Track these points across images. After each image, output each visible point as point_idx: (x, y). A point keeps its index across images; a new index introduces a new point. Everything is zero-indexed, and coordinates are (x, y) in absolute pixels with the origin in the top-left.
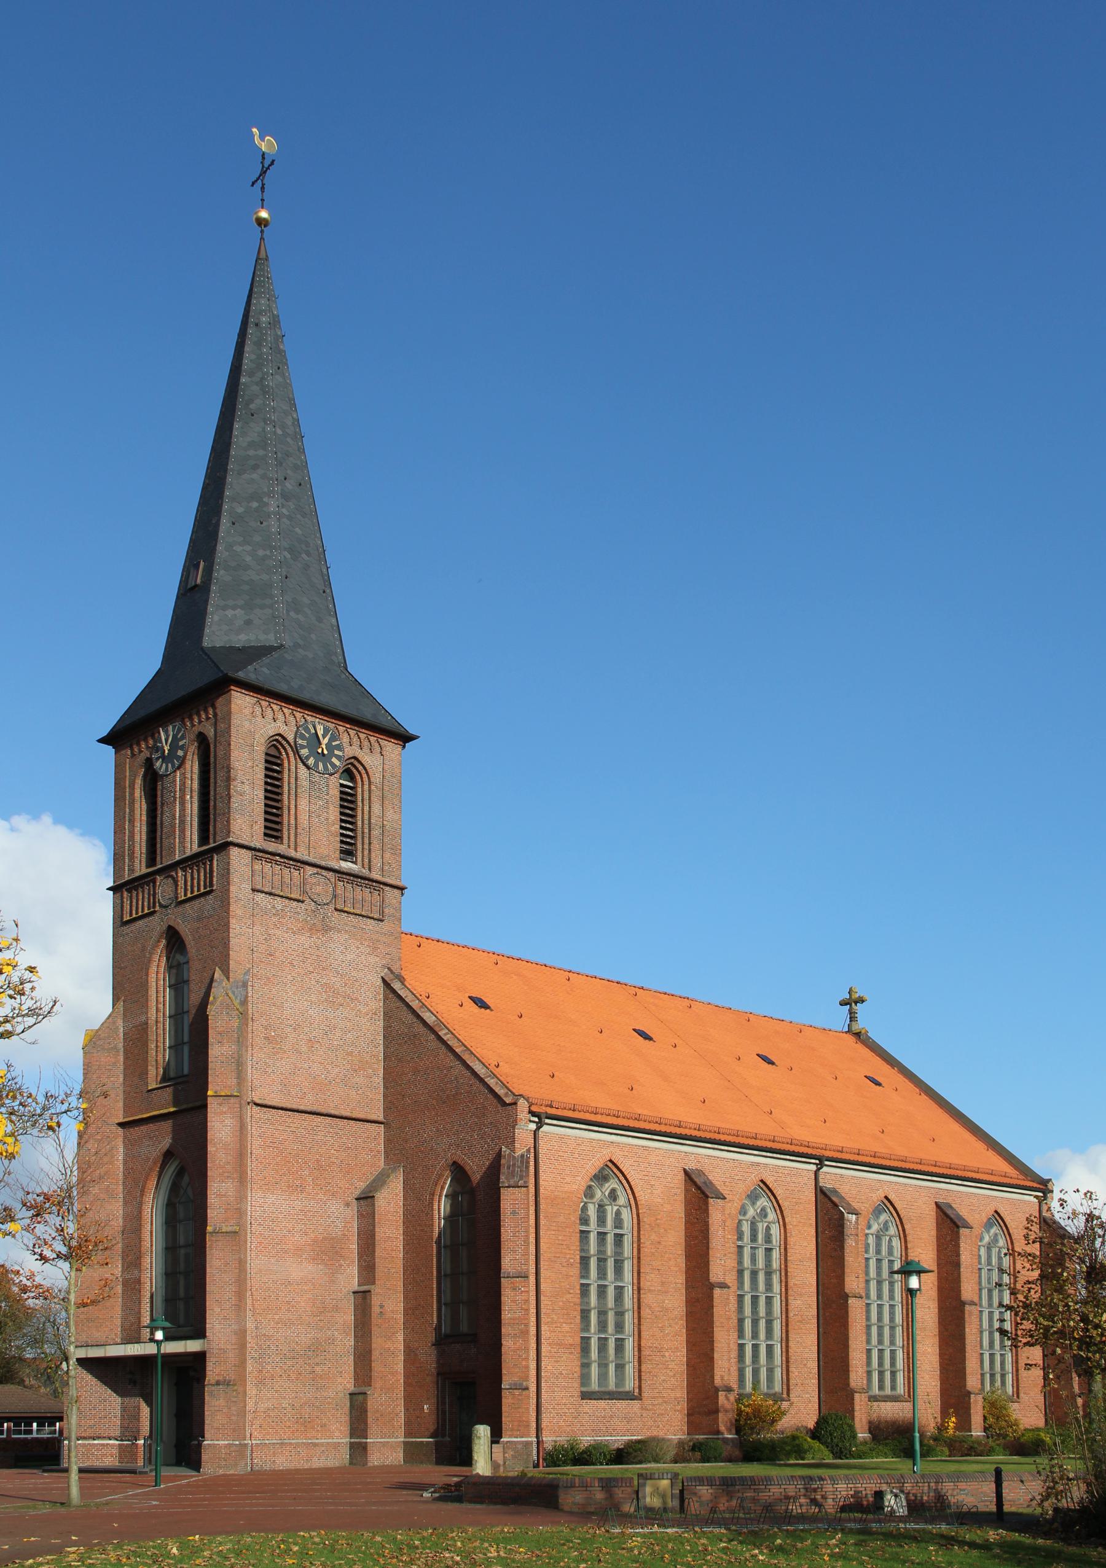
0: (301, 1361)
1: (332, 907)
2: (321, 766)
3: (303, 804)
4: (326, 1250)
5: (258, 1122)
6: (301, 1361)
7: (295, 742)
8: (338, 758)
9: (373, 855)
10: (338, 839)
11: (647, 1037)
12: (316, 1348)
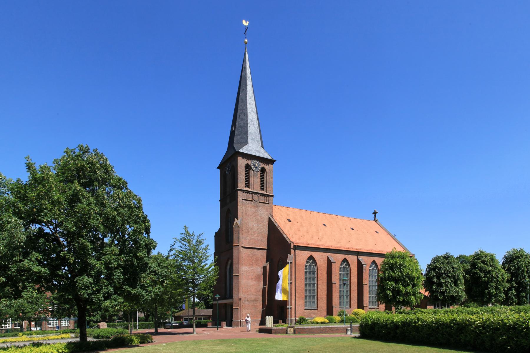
3: (252, 179)
5: (243, 252)
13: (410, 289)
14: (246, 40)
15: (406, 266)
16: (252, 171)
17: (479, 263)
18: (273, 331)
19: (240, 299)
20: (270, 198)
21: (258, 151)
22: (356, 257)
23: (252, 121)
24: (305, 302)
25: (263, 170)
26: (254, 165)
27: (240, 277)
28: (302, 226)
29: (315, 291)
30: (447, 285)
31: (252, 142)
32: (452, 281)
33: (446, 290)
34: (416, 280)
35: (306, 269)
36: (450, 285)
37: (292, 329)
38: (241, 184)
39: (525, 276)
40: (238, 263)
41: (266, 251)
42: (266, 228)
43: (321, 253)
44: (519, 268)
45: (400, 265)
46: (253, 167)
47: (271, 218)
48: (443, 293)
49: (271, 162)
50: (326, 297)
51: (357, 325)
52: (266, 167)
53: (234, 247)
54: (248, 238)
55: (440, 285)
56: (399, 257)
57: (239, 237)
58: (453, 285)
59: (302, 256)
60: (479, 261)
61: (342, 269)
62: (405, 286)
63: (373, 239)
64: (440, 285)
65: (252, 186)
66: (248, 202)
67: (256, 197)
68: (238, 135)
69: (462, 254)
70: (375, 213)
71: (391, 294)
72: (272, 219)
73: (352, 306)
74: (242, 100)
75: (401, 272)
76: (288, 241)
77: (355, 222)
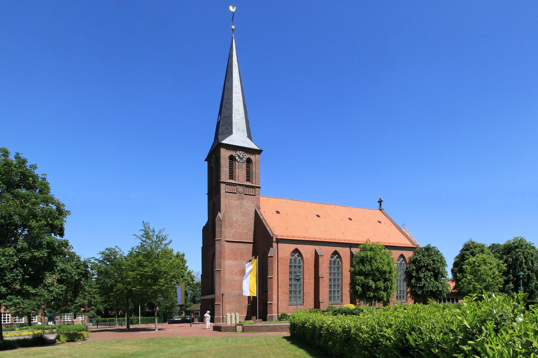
3: (237, 171)
5: (227, 245)
11: (380, 222)
13: (381, 284)
14: (233, 27)
15: (376, 259)
16: (237, 163)
17: (467, 255)
18: (222, 329)
19: (223, 295)
20: (257, 189)
21: (243, 141)
22: (348, 249)
23: (238, 110)
24: (290, 297)
25: (249, 161)
26: (239, 156)
27: (222, 272)
28: (291, 216)
29: (302, 286)
30: (426, 279)
31: (237, 133)
32: (431, 275)
33: (425, 284)
34: (387, 274)
35: (291, 263)
36: (430, 279)
37: (241, 327)
38: (224, 176)
39: (524, 268)
40: (220, 257)
41: (252, 245)
42: (252, 221)
43: (308, 246)
44: (517, 259)
45: (371, 258)
46: (237, 158)
47: (257, 210)
48: (422, 288)
49: (259, 152)
50: (313, 291)
51: (287, 323)
52: (252, 157)
53: (216, 242)
54: (233, 231)
55: (419, 279)
56: (371, 249)
57: (221, 231)
58: (433, 279)
59: (286, 250)
60: (468, 252)
61: (332, 262)
62: (375, 281)
63: (369, 228)
64: (419, 279)
65: (237, 178)
66: (232, 194)
67: (241, 189)
68: (223, 126)
69: (496, 243)
70: (380, 202)
71: (360, 290)
72: (258, 212)
73: (344, 302)
74: (228, 89)
75: (371, 266)
76: (271, 234)
77: (354, 212)
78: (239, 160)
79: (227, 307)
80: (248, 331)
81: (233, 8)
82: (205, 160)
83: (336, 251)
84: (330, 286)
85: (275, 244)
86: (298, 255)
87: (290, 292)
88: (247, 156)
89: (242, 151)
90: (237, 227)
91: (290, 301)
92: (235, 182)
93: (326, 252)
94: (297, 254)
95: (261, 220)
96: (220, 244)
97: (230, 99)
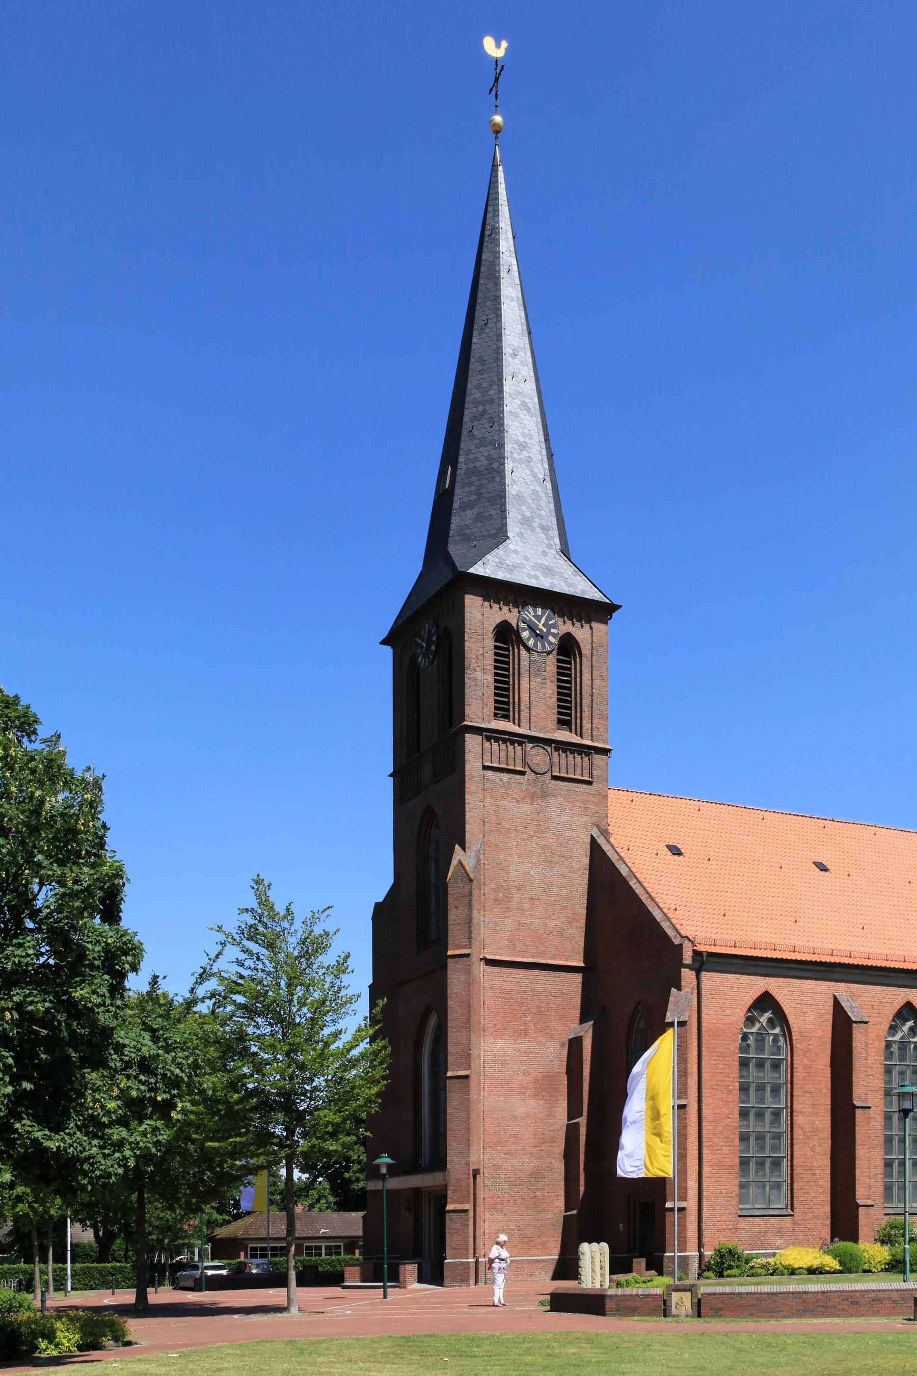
0: (524, 1187)
1: (549, 775)
2: (539, 645)
4: (543, 1087)
5: (487, 977)
6: (524, 1187)
7: (518, 626)
8: (554, 635)
9: (584, 722)
10: (555, 711)
11: (824, 869)
12: (536, 1175)
14: (498, 119)
16: (524, 652)
18: (609, 1305)
19: (476, 1173)
20: (598, 759)
21: (548, 571)
23: (523, 447)
24: (742, 1186)
25: (568, 648)
26: (532, 628)
27: (473, 1082)
29: (784, 1141)
31: (521, 535)
35: (744, 1049)
40: (467, 1024)
41: (578, 978)
42: (581, 883)
46: (525, 634)
47: (601, 840)
49: (601, 611)
50: (826, 1162)
52: (581, 633)
53: (451, 963)
54: (509, 923)
57: (469, 922)
61: (894, 1048)
65: (525, 714)
66: (505, 777)
67: (538, 756)
68: (465, 507)
72: (605, 847)
74: (482, 362)
76: (671, 933)
78: (531, 643)
79: (488, 1222)
80: (717, 1312)
81: (498, 46)
82: (384, 642)
83: (908, 1005)
84: (888, 1140)
85: (688, 975)
86: (770, 1020)
87: (744, 1163)
88: (565, 627)
89: (544, 608)
90: (527, 906)
91: (742, 1199)
92: (515, 729)
93: (874, 1005)
94: (768, 1015)
95: (623, 882)
96: (468, 972)
97: (491, 401)
